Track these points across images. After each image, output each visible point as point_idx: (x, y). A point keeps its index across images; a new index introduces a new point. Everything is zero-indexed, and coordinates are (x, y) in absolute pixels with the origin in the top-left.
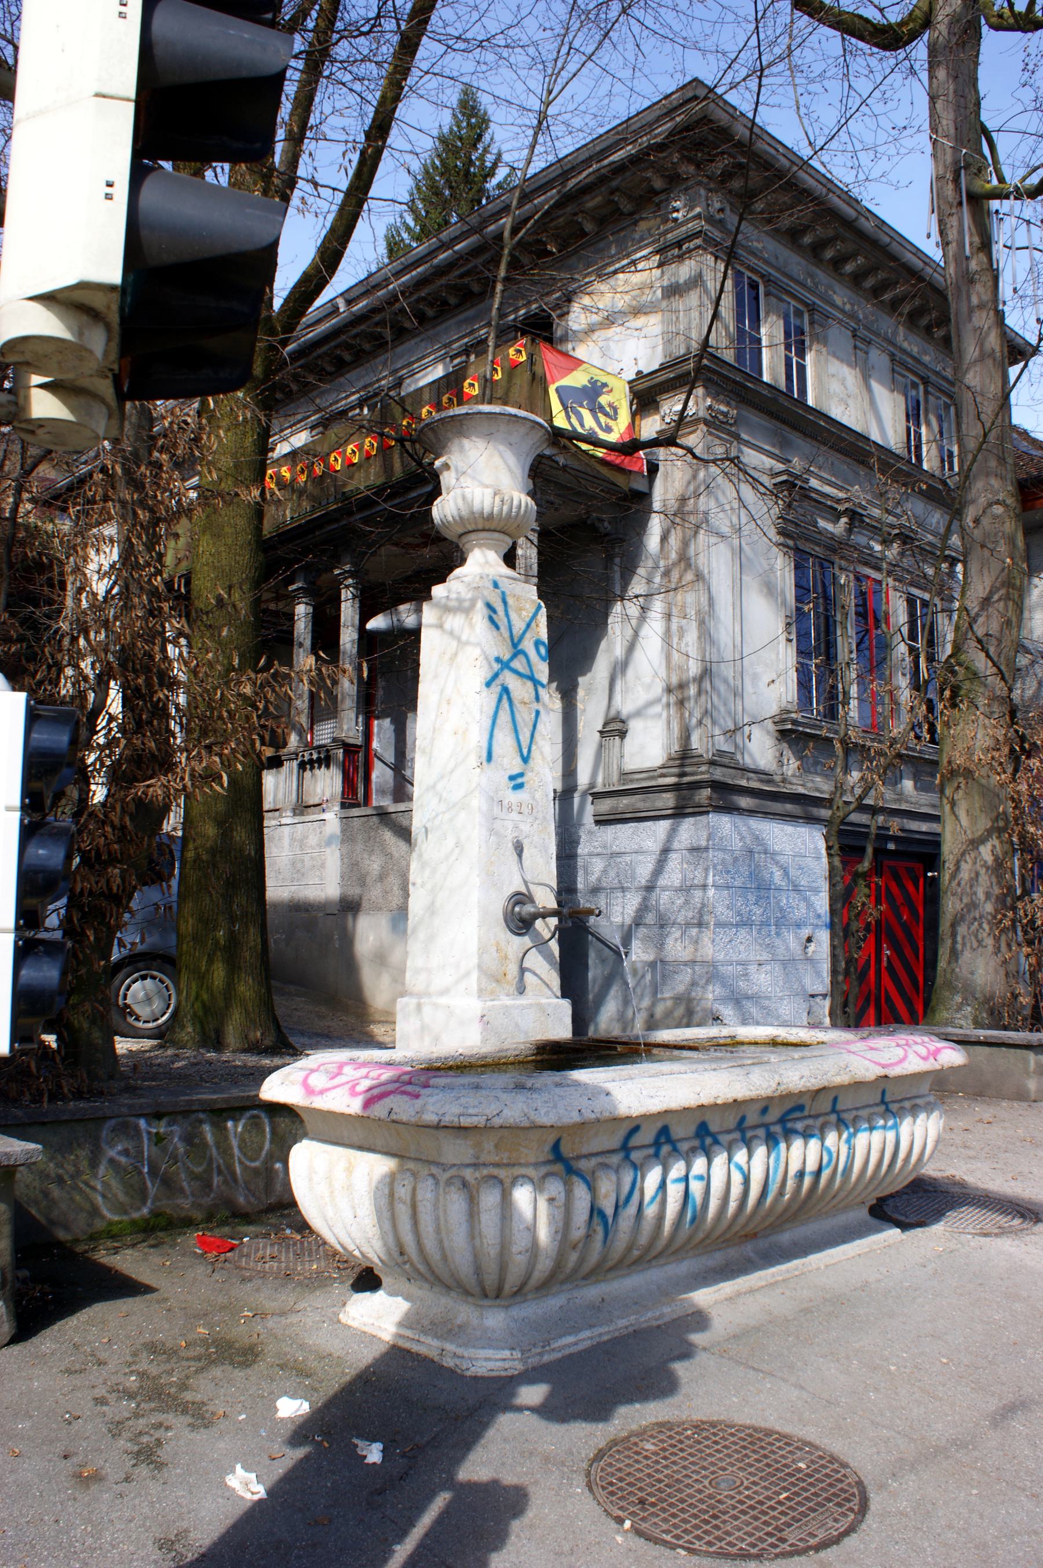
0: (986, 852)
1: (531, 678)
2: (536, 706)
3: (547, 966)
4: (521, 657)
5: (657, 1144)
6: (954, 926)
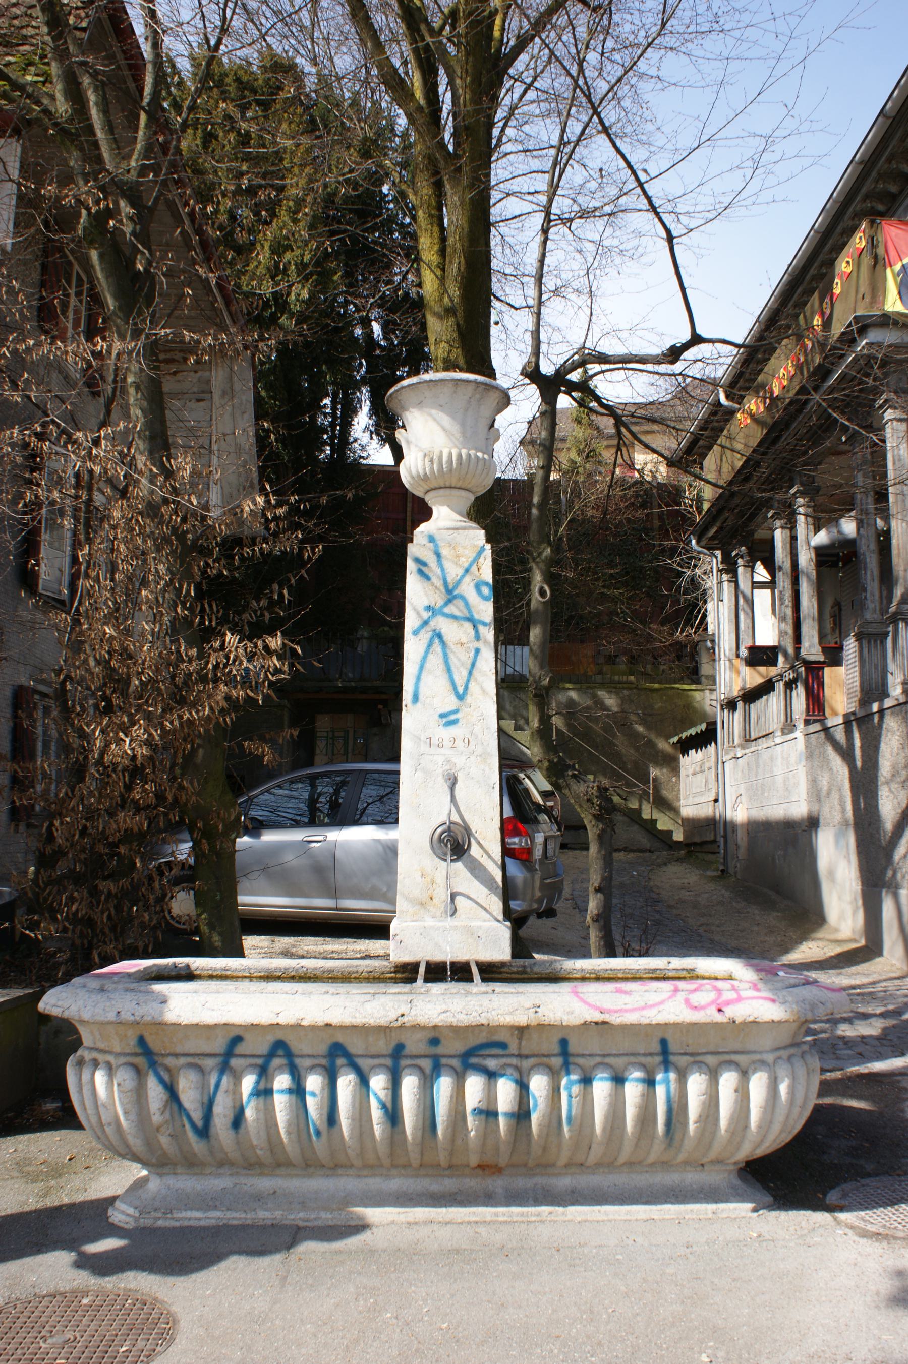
1: (470, 619)
2: (476, 645)
3: (485, 891)
4: (459, 603)
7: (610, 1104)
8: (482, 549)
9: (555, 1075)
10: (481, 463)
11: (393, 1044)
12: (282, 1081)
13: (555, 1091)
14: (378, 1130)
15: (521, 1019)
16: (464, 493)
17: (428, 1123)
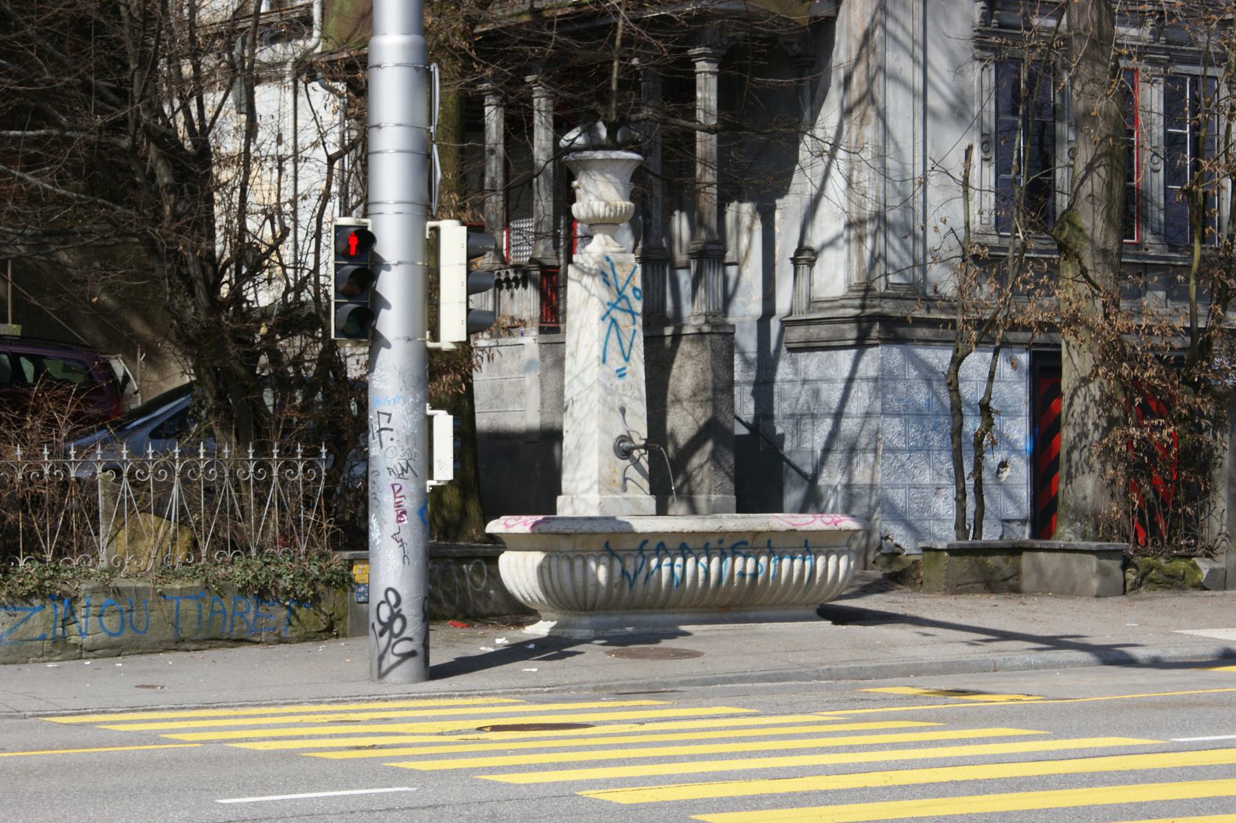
0: (1094, 389)
4: (623, 301)
5: (657, 550)
6: (1069, 453)
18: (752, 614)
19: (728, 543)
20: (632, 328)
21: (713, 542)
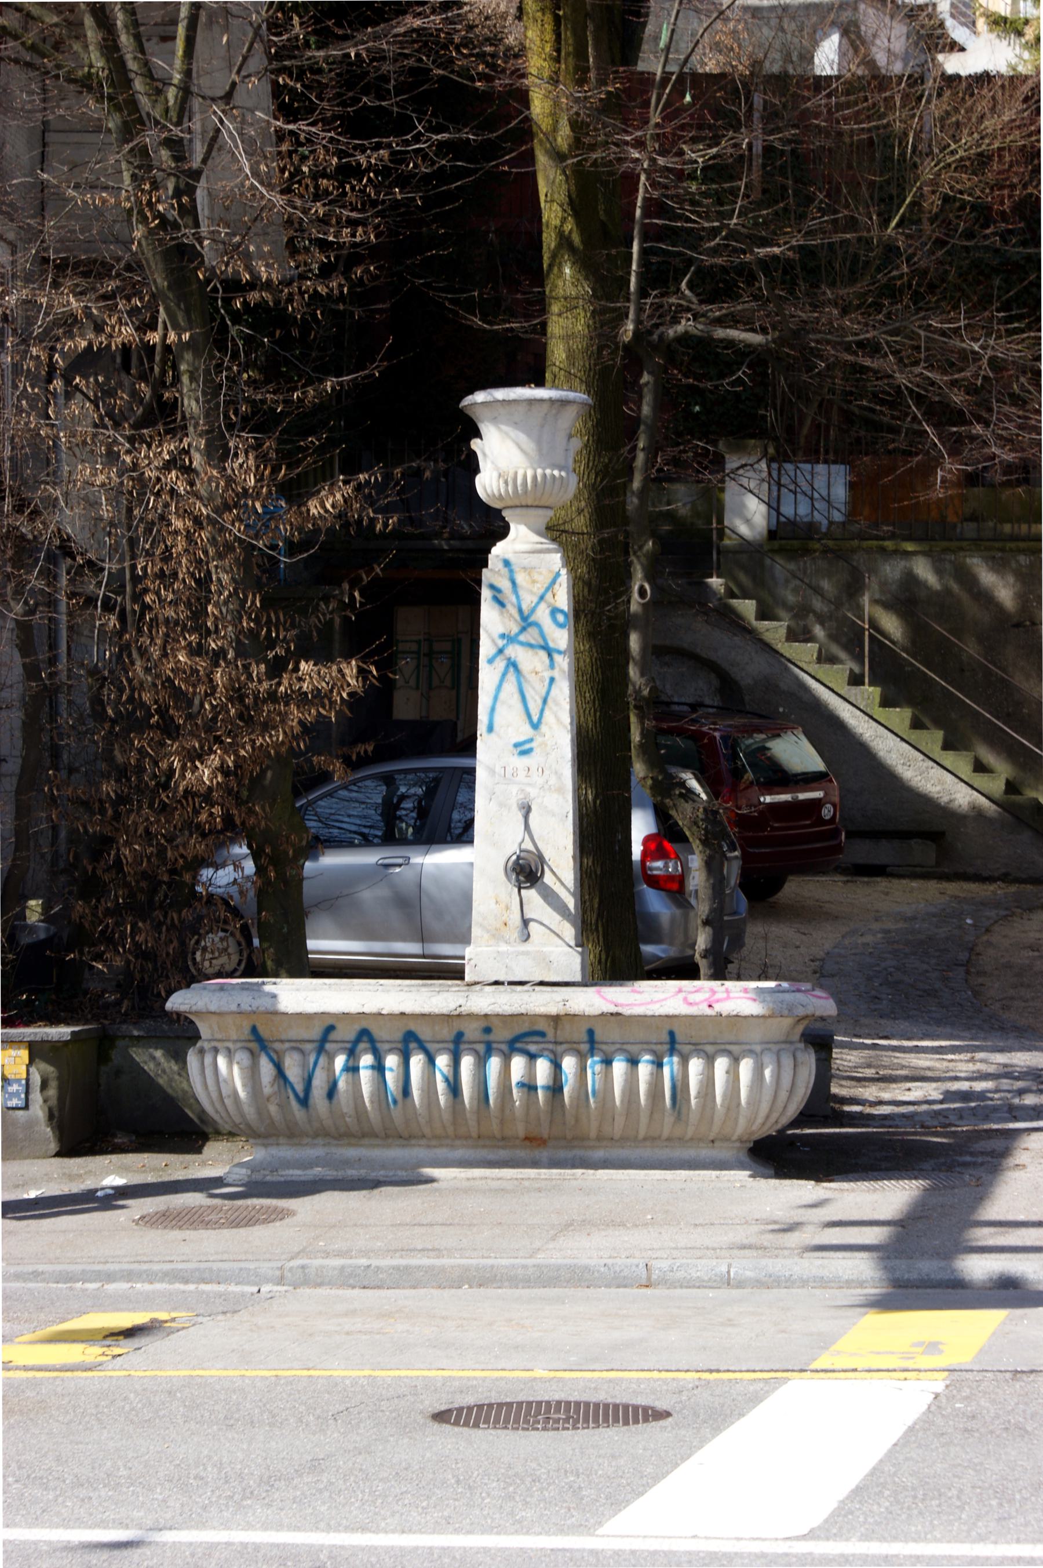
4: (533, 631)
7: (626, 1081)
8: (558, 574)
9: (582, 1058)
10: (558, 483)
11: (455, 1032)
12: (366, 1060)
13: (583, 1069)
14: (442, 1099)
15: (553, 1010)
16: (541, 512)
17: (482, 1095)
18: (599, 1154)
19: (502, 1034)
20: (547, 675)
21: (472, 1031)
